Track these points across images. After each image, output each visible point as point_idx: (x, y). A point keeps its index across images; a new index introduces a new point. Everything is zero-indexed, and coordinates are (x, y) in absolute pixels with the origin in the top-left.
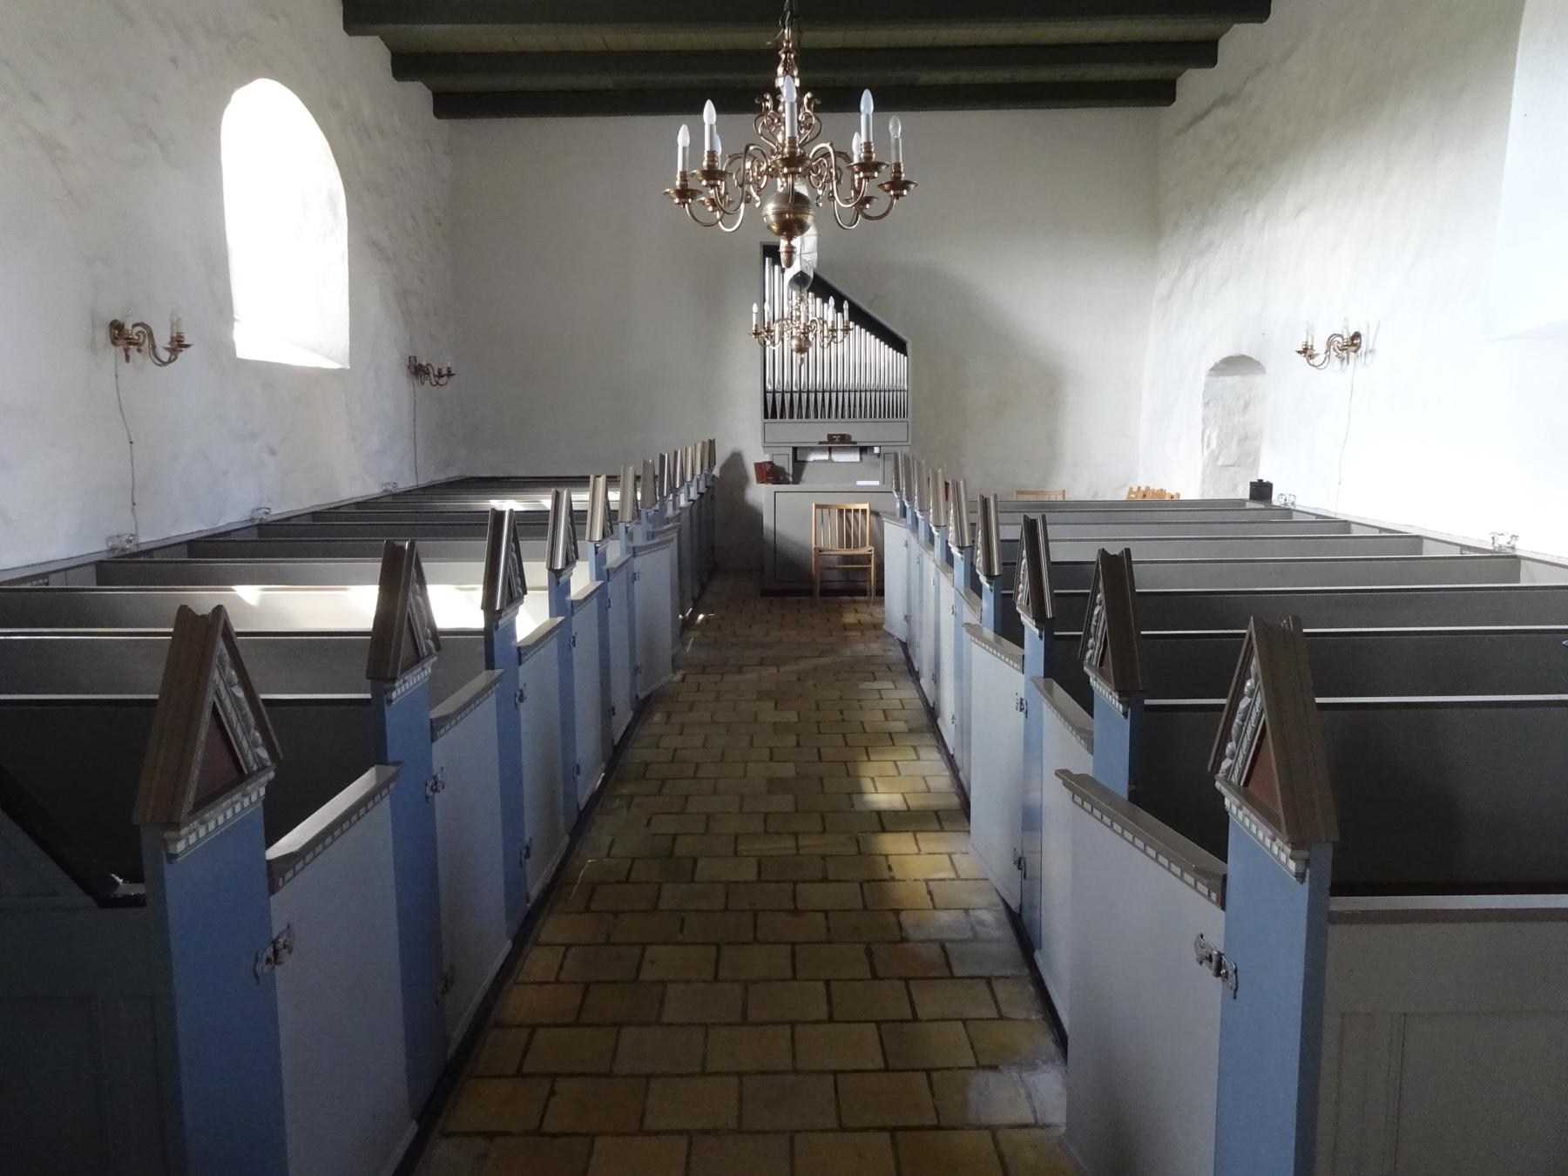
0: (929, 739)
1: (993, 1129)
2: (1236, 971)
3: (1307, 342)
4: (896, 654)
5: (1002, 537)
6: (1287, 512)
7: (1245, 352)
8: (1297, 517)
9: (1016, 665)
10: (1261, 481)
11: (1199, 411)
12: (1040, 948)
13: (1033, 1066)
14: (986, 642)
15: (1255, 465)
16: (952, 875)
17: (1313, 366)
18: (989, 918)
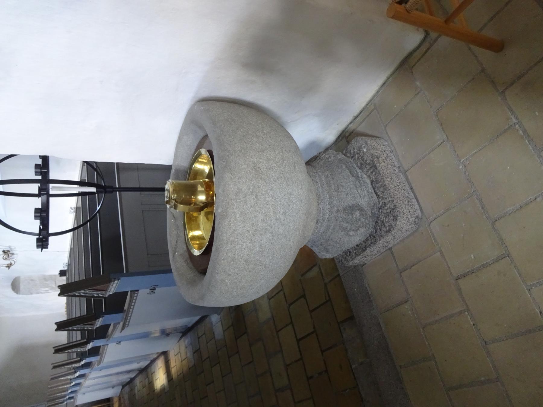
0: (149, 370)
1: (224, 331)
2: (152, 286)
3: (5, 266)
4: (127, 388)
5: (76, 357)
6: (69, 265)
7: (10, 284)
8: (70, 263)
9: (106, 347)
10: (59, 274)
11: (34, 295)
12: (187, 325)
13: (212, 323)
14: (101, 358)
15: (55, 275)
16: (179, 354)
17: (15, 263)
18: (185, 341)
